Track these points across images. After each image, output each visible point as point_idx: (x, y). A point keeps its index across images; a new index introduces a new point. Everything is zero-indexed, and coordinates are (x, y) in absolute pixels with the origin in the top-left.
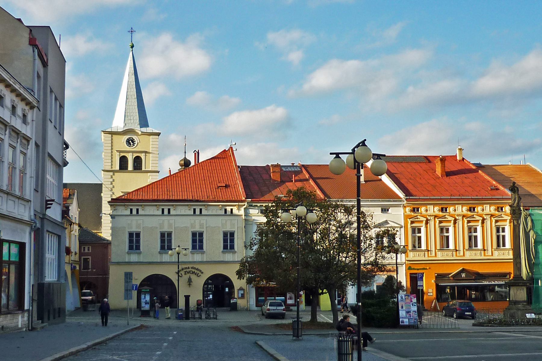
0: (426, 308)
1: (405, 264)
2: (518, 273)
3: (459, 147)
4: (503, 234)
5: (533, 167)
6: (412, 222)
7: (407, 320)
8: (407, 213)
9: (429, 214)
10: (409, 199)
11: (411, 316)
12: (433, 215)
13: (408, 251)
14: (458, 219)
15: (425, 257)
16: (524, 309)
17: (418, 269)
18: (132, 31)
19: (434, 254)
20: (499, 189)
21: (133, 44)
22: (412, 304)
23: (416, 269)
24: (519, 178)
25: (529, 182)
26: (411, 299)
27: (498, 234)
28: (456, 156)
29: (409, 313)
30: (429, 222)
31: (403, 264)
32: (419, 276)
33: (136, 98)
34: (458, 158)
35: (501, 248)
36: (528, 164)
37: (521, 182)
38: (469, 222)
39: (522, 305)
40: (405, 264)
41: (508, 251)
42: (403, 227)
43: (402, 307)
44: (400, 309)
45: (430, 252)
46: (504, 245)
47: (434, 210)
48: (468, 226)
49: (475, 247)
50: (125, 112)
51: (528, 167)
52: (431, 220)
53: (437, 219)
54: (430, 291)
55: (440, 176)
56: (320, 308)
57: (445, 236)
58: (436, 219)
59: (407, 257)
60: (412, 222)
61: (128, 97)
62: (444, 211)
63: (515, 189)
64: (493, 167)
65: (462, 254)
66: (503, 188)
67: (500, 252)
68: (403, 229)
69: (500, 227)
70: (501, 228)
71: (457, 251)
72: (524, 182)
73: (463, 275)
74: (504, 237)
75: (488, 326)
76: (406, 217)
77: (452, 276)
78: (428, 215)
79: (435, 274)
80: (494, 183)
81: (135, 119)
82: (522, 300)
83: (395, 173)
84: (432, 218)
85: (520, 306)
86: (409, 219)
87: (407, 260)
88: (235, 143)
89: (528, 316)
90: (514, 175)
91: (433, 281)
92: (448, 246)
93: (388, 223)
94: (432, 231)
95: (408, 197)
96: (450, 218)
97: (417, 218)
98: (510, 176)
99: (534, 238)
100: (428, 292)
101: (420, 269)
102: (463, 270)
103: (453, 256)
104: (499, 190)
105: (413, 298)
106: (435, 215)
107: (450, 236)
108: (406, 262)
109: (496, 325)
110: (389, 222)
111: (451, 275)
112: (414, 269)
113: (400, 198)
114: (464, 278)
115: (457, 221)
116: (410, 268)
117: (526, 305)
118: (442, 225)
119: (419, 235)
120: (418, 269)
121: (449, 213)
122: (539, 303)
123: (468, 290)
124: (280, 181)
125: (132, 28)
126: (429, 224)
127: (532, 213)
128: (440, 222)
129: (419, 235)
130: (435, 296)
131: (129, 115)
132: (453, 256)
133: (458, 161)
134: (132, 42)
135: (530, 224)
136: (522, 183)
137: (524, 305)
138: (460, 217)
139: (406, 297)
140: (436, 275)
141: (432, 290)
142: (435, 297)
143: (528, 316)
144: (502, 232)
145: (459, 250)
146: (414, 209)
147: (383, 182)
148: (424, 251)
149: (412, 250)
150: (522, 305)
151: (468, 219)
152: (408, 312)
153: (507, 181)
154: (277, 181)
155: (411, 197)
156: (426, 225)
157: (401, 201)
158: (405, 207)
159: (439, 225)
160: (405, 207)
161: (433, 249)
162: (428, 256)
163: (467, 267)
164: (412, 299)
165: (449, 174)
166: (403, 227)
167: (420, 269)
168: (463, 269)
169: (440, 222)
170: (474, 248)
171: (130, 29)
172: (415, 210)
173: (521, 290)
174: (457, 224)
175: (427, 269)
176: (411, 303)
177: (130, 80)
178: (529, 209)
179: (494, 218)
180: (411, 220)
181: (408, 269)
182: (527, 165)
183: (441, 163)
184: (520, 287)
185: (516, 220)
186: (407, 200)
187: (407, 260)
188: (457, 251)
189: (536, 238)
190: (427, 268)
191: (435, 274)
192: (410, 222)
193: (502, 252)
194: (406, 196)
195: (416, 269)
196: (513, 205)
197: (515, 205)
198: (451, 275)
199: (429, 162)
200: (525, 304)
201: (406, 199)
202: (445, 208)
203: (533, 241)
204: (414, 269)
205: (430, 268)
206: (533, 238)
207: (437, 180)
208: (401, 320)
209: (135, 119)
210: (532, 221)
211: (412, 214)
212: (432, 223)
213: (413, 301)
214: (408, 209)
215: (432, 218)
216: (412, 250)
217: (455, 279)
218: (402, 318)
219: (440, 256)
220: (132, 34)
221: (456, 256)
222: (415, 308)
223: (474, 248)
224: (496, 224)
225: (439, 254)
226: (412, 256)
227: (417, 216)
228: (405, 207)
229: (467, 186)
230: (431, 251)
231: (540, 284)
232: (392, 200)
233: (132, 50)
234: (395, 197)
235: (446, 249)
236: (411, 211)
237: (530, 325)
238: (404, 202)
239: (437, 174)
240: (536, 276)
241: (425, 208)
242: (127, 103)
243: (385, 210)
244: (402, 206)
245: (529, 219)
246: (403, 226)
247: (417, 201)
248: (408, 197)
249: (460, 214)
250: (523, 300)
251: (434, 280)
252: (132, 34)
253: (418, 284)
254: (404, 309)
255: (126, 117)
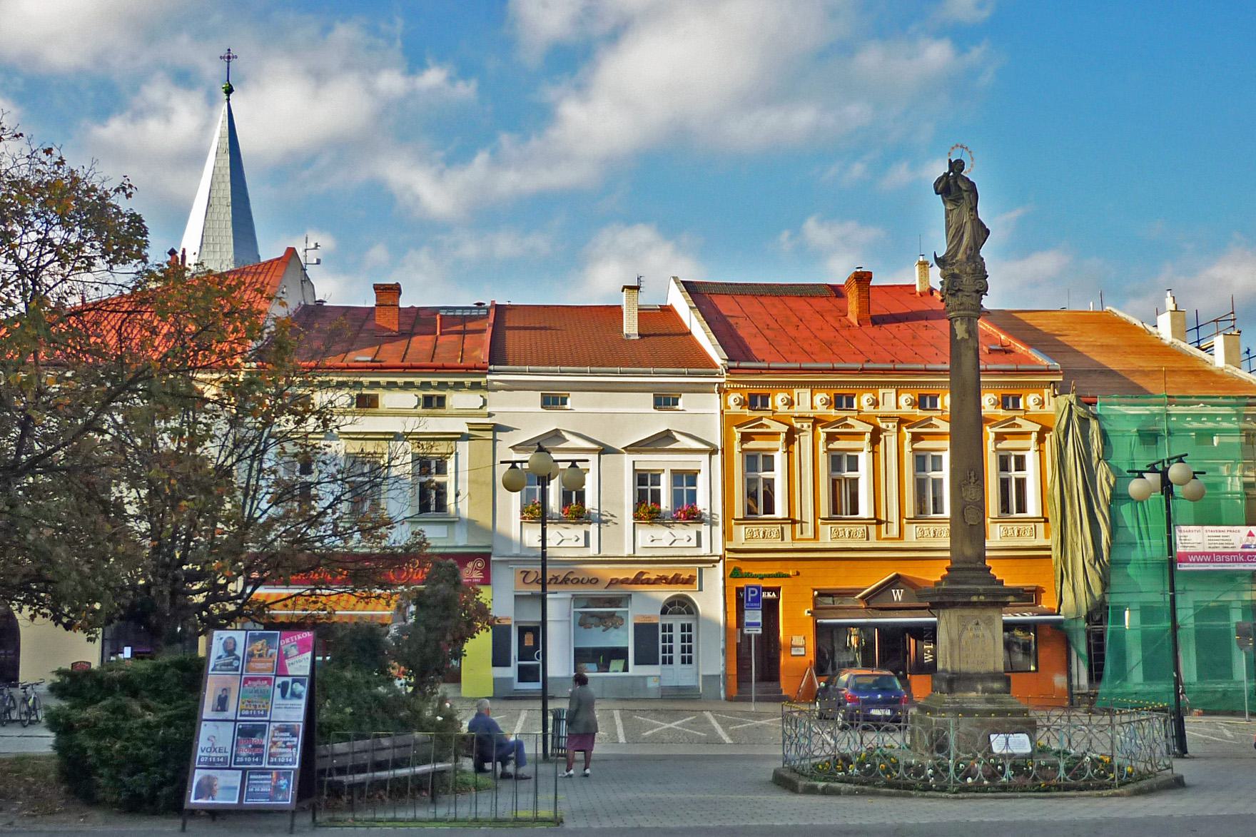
0: (784, 694)
1: (721, 561)
2: (969, 551)
3: (921, 259)
4: (1020, 474)
5: (1121, 314)
6: (746, 438)
7: (234, 778)
8: (732, 409)
9: (797, 415)
10: (738, 368)
11: (261, 756)
12: (809, 418)
13: (733, 521)
14: (885, 431)
15: (783, 539)
16: (989, 713)
17: (762, 578)
18: (229, 57)
19: (809, 533)
20: (1013, 352)
21: (230, 85)
22: (284, 687)
23: (755, 577)
24: (1081, 336)
25: (1107, 346)
26: (282, 657)
27: (1004, 475)
28: (915, 286)
29: (255, 740)
30: (796, 436)
31: (718, 561)
32: (750, 595)
33: (229, 204)
34: (918, 289)
35: (1012, 516)
36: (1108, 308)
37: (1084, 344)
38: (916, 438)
39: (984, 691)
40: (721, 561)
41: (1033, 525)
42: (720, 452)
43: (222, 704)
44: (207, 711)
45: (798, 526)
46: (1022, 508)
47: (811, 402)
48: (914, 450)
49: (934, 513)
50: (203, 236)
51: (1109, 316)
52: (803, 431)
53: (823, 427)
54: (797, 640)
55: (856, 323)
56: (460, 691)
57: (846, 479)
58: (819, 429)
59: (730, 539)
60: (746, 438)
61: (211, 202)
62: (844, 407)
63: (960, 189)
64: (1014, 314)
65: (894, 531)
66: (1023, 348)
67: (1009, 526)
68: (717, 459)
69: (1011, 455)
70: (1013, 459)
71: (879, 522)
72: (1094, 346)
73: (898, 595)
74: (1021, 483)
75: (812, 790)
76: (729, 421)
77: (862, 598)
78: (795, 417)
79: (814, 590)
80: (1003, 337)
81: (224, 250)
82: (982, 669)
83: (732, 316)
84: (805, 425)
85: (974, 694)
86: (738, 427)
87: (726, 549)
88: (317, 245)
89: (998, 743)
90: (1068, 330)
91: (806, 612)
92: (855, 510)
93: (675, 441)
94: (806, 465)
95: (735, 364)
96: (860, 427)
97: (762, 425)
98: (1057, 333)
99: (1112, 483)
100: (793, 646)
101: (769, 576)
102: (896, 581)
103: (868, 539)
104: (1012, 355)
105: (294, 651)
106: (814, 418)
107: (860, 480)
108: (727, 556)
109: (849, 786)
110: (678, 437)
111: (860, 595)
112: (749, 576)
113: (709, 363)
114: (902, 605)
115: (882, 436)
116: (736, 574)
117: (998, 692)
118: (836, 445)
119: (767, 475)
120: (762, 578)
121: (859, 412)
122: (1125, 680)
123: (913, 641)
124: (397, 330)
125: (229, 50)
126: (797, 443)
127: (1103, 413)
128: (831, 438)
129: (767, 475)
130: (811, 657)
131: (211, 241)
132: (868, 539)
133: (918, 294)
134: (228, 80)
135: (1096, 444)
136: (1087, 346)
137: (992, 691)
138: (891, 425)
139: (259, 644)
140: (816, 593)
141: (802, 640)
142: (813, 659)
143: (998, 743)
144: (1016, 470)
145: (887, 522)
146: (753, 398)
147: (694, 338)
148: (782, 521)
149: (744, 519)
150: (984, 691)
151: (915, 430)
152: (248, 732)
153: (1046, 341)
154: (389, 330)
155: (743, 364)
156: (788, 446)
157: (712, 375)
158: (723, 391)
159: (827, 445)
160: (726, 391)
161: (809, 516)
162: (793, 538)
163: (909, 572)
164: (286, 657)
165: (877, 321)
166: (720, 452)
167: (769, 576)
168: (897, 577)
169: (831, 438)
170: (932, 516)
171: (224, 53)
172: (756, 401)
173: (982, 626)
174: (882, 443)
175: (788, 576)
176: (279, 680)
177: (219, 165)
178: (1096, 403)
179: (991, 427)
180: (742, 430)
181: (731, 576)
182: (1107, 312)
183: (858, 287)
184: (976, 612)
185: (962, 317)
186: (731, 371)
187: (730, 550)
188: (879, 522)
189: (1115, 483)
190: (791, 574)
191: (814, 590)
192: (738, 436)
193: (1016, 527)
194: (728, 360)
195: (755, 577)
196: (955, 255)
197: (961, 256)
198: (860, 595)
199: (837, 297)
200: (997, 686)
201: (729, 370)
202: (847, 398)
203: (1108, 492)
204: (749, 576)
205: (798, 574)
206: (1109, 485)
207: (845, 333)
208: (198, 776)
209: (224, 250)
210: (1104, 435)
211: (747, 412)
212: (806, 440)
213: (291, 671)
214: (733, 398)
215: (805, 425)
216: (744, 519)
217: (873, 605)
218: (211, 765)
219: (828, 537)
220: (228, 62)
221: (879, 537)
222: (294, 712)
223: (932, 516)
224: (999, 446)
225: (826, 530)
226: (742, 536)
227: (761, 418)
228: (726, 391)
229: (924, 345)
230: (801, 522)
231: (1127, 624)
232: (685, 370)
233: (228, 100)
234: (700, 361)
235: (849, 516)
236: (742, 404)
237: (1004, 788)
238: (721, 376)
239: (848, 320)
240: (1113, 600)
241: (786, 395)
242: (209, 215)
243: (665, 401)
244: (716, 390)
245: (1094, 425)
246: (719, 448)
247: (761, 373)
248: (735, 364)
249: (892, 414)
250: (991, 668)
251: (811, 608)
252: (228, 62)
253: (747, 620)
254: (230, 713)
255: (204, 245)
